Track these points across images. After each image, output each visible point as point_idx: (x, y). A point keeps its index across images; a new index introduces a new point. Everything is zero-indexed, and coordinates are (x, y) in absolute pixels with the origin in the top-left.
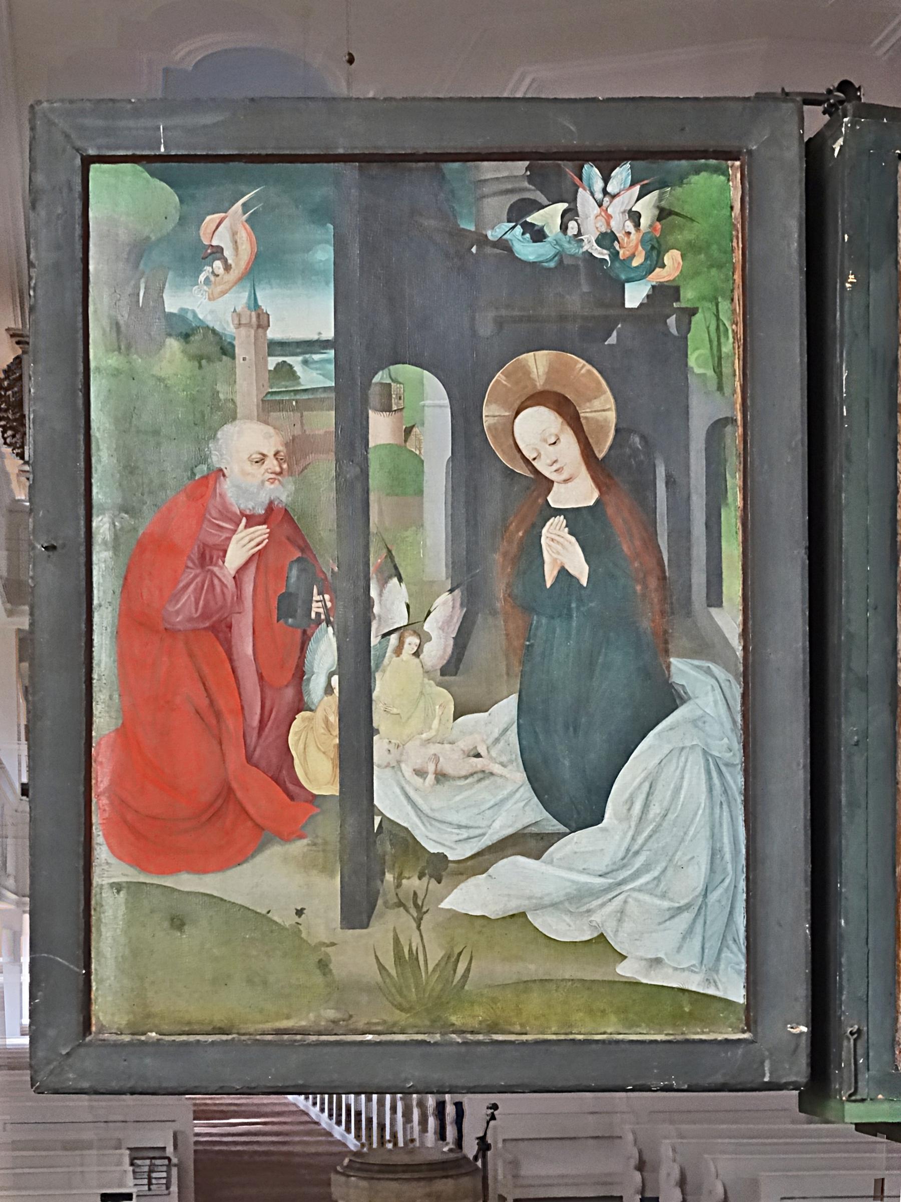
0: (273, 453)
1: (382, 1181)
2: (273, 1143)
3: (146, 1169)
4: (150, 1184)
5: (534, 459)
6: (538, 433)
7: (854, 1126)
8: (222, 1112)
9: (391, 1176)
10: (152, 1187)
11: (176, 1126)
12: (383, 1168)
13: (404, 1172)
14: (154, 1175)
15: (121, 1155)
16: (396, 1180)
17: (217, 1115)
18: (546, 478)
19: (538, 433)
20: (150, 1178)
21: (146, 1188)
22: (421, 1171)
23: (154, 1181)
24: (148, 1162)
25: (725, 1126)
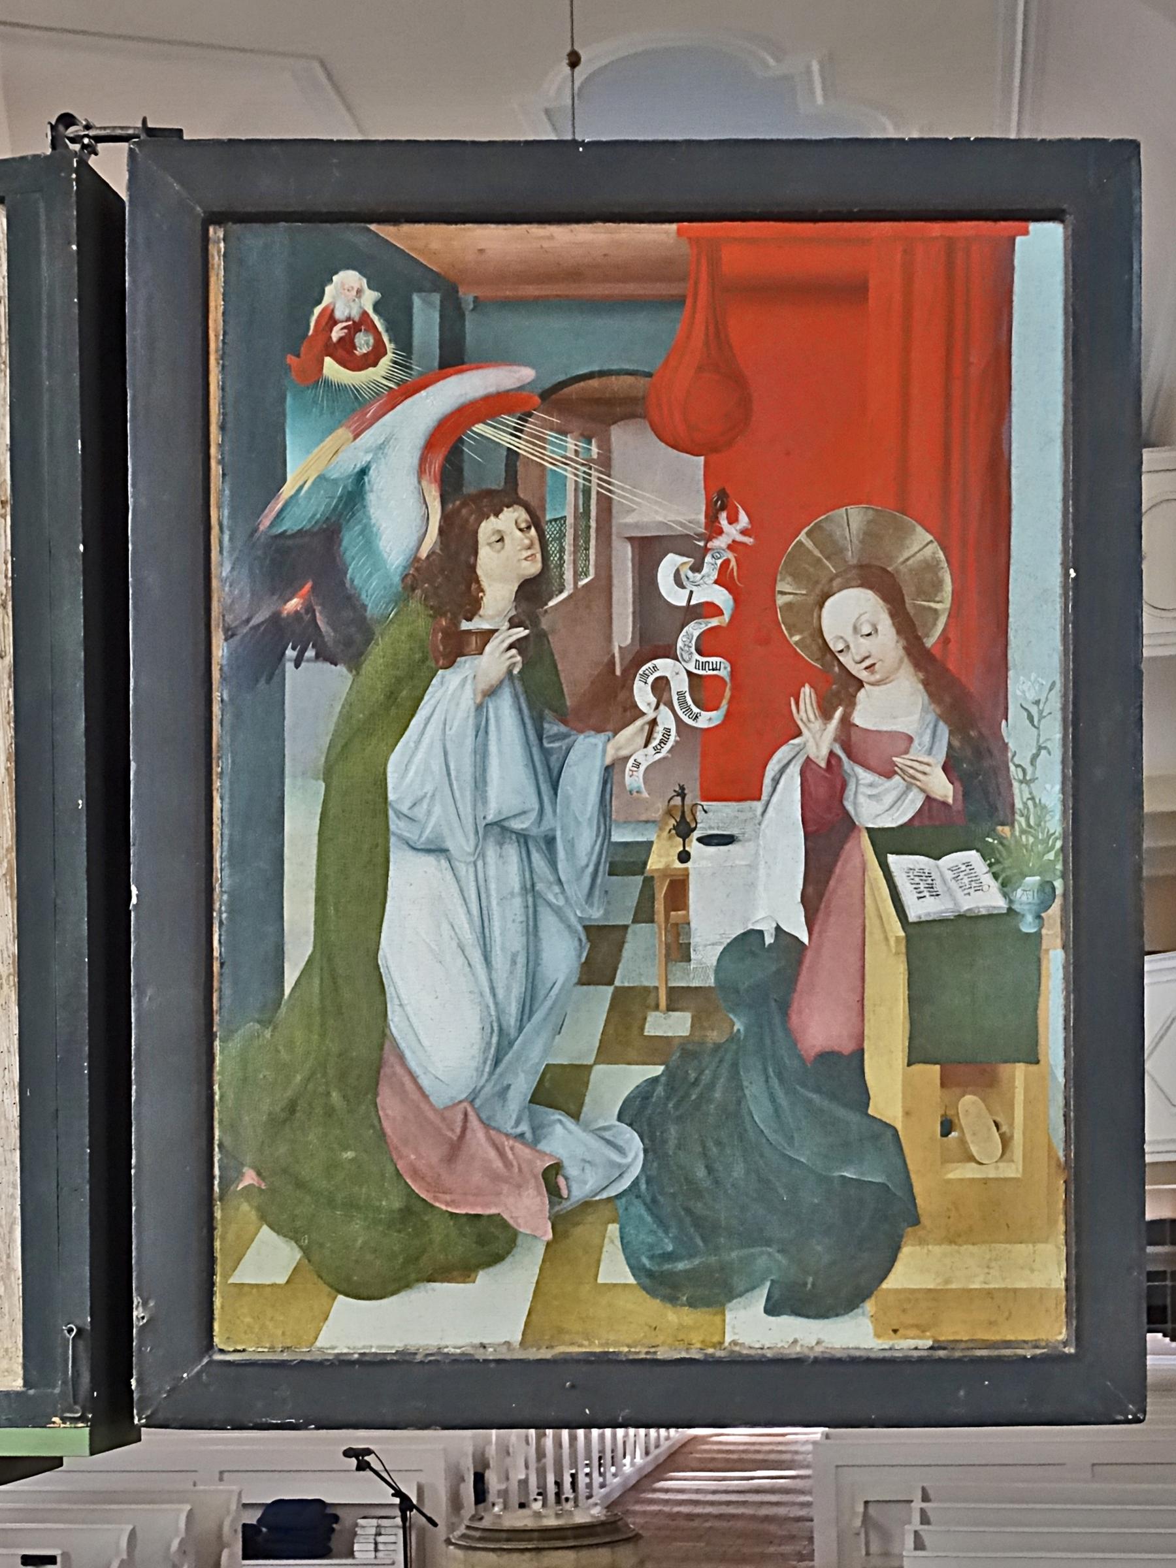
0: (850, 629)
1: (545, 1553)
2: (728, 1503)
3: (373, 1531)
4: (376, 1550)
5: (841, 651)
6: (853, 619)
7: (523, 1477)
8: (754, 1461)
9: (586, 1542)
10: (380, 1554)
11: (422, 1478)
12: (486, 1534)
13: (508, 1540)
14: (380, 1539)
15: (180, 1510)
16: (493, 1550)
17: (739, 1465)
18: (410, 721)
19: (853, 619)
20: (376, 1544)
21: (372, 1554)
22: (530, 1540)
23: (381, 1547)
24: (374, 1522)
25: (1145, 1486)
